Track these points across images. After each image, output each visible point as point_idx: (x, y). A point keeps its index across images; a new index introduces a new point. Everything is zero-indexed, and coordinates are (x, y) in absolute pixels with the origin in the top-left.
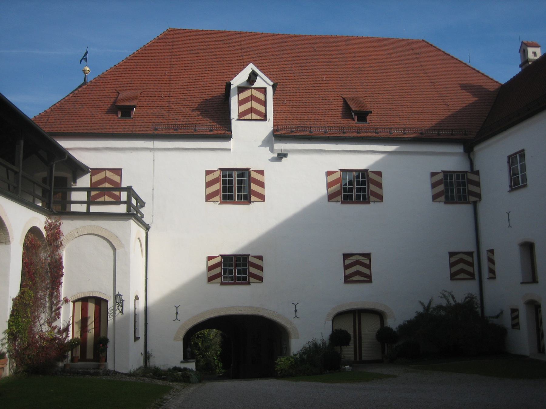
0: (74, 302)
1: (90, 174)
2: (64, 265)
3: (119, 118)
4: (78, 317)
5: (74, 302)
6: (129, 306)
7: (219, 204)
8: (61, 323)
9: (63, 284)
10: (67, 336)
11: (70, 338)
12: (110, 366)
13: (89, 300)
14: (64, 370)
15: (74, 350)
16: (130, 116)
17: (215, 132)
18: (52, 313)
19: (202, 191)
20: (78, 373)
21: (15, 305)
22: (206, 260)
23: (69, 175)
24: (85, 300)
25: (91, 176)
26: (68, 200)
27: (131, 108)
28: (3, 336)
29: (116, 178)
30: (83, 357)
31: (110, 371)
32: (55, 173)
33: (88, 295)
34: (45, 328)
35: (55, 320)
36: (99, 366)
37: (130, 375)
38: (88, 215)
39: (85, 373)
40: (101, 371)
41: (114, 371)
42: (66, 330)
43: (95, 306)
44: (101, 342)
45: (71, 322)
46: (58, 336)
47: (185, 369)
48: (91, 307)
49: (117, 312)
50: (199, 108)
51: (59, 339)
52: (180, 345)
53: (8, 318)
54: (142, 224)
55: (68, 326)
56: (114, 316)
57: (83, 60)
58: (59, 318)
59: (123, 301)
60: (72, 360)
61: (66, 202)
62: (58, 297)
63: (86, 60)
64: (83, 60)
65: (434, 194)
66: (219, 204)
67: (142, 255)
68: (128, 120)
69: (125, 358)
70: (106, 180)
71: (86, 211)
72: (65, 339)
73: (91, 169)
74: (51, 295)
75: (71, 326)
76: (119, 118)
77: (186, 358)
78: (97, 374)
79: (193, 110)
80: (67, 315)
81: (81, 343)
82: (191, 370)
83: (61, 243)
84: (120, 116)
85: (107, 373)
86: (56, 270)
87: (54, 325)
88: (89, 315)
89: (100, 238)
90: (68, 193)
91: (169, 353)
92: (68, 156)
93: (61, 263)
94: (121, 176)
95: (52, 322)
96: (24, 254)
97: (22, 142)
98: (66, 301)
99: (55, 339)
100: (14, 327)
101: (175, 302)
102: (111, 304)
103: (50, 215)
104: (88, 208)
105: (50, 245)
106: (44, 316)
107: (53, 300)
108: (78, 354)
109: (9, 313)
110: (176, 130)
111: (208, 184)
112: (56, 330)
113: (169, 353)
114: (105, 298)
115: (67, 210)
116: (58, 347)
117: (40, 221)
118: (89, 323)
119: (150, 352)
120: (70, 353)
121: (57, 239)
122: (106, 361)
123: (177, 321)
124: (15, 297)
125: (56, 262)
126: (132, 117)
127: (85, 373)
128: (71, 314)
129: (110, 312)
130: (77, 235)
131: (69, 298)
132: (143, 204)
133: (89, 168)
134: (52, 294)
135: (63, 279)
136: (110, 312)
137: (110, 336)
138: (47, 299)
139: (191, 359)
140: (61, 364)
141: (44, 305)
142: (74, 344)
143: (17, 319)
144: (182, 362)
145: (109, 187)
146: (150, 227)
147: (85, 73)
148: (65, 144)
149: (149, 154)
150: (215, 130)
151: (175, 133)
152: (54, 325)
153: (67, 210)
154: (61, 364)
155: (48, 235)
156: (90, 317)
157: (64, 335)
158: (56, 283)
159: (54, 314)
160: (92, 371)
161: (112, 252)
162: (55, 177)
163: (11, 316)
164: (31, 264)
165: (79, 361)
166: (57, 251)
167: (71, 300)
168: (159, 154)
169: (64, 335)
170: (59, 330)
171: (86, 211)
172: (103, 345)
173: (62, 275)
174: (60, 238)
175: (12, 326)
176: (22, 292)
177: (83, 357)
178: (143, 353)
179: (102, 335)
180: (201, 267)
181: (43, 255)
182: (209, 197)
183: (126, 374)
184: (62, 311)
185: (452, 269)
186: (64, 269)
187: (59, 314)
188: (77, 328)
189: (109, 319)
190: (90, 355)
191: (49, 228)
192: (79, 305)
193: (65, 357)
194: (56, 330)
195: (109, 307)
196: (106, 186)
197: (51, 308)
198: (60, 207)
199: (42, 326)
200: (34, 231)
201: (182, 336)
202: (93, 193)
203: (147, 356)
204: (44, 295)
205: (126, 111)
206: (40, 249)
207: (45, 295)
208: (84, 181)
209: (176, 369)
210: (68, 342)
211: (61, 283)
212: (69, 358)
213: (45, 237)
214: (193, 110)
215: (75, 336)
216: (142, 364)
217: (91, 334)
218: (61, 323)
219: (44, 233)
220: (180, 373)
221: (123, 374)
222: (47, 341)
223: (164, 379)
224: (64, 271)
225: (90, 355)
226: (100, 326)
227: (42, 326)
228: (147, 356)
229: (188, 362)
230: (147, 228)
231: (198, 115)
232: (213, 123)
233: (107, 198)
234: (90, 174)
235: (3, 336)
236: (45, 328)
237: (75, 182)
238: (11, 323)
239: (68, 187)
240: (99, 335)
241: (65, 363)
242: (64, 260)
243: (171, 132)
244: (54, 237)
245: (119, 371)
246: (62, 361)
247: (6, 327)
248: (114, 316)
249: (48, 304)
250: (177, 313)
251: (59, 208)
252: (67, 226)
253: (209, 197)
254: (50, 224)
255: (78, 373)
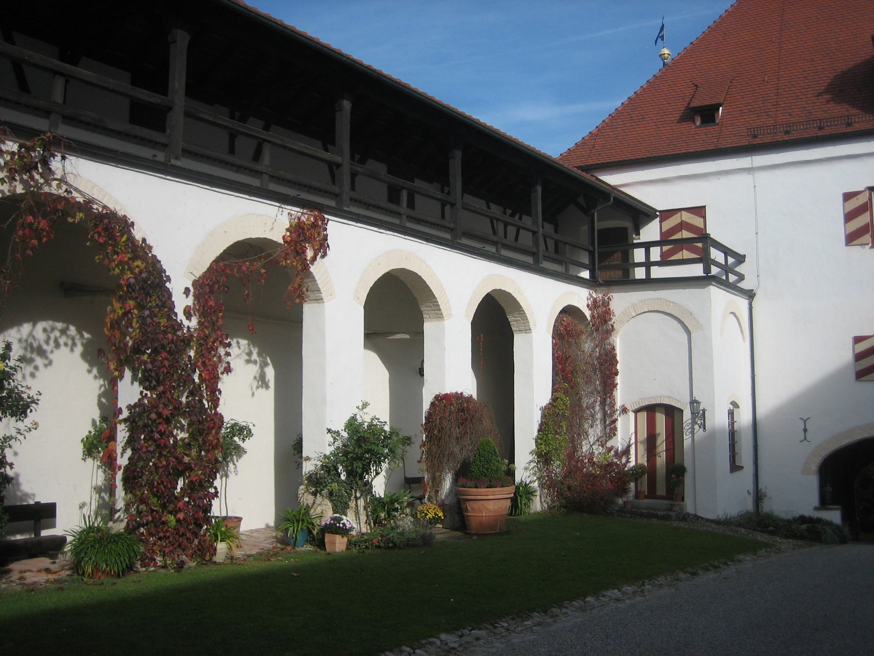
0: (636, 412)
1: (658, 219)
2: (618, 358)
3: (698, 127)
4: (643, 434)
5: (636, 412)
6: (718, 419)
7: (871, 247)
8: (619, 442)
9: (618, 387)
10: (628, 461)
11: (632, 464)
12: (689, 508)
13: (657, 409)
14: (622, 511)
15: (639, 481)
16: (714, 121)
17: (857, 127)
18: (605, 428)
19: (839, 229)
20: (641, 515)
21: (543, 416)
22: (851, 342)
23: (628, 224)
24: (651, 409)
25: (661, 222)
26: (630, 261)
27: (716, 108)
28: (530, 458)
29: (697, 221)
30: (652, 493)
31: (688, 514)
32: (598, 226)
33: (653, 402)
34: (598, 450)
35: (610, 437)
36: (672, 505)
37: (718, 522)
38: (649, 282)
39: (649, 516)
40: (673, 514)
41: (695, 515)
42: (626, 452)
43: (663, 417)
44: (676, 472)
45: (633, 441)
46: (615, 460)
47: (819, 520)
48: (661, 419)
49: (696, 427)
50: (827, 91)
51: (616, 464)
52: (813, 481)
53: (536, 433)
54: (736, 291)
55: (629, 446)
56: (693, 433)
57: (659, 39)
58: (615, 435)
59: (704, 411)
60: (637, 495)
61: (628, 264)
62: (612, 405)
63: (662, 38)
64: (659, 39)
65: (848, 232)
66: (871, 247)
67: (744, 338)
68: (710, 129)
69: (717, 495)
70: (682, 225)
71: (644, 277)
72: (625, 465)
73: (660, 211)
74: (603, 403)
75: (633, 446)
76: (698, 127)
77: (824, 503)
78: (667, 518)
79: (819, 95)
80: (627, 431)
81: (648, 472)
82: (829, 523)
83: (612, 326)
84: (698, 123)
85: (685, 517)
86: (607, 367)
87: (609, 444)
88: (658, 431)
89: (667, 317)
90: (630, 251)
91: (797, 494)
92: (615, 198)
93: (614, 356)
94: (704, 217)
95: (606, 441)
96: (554, 346)
97: (539, 189)
98: (624, 410)
99: (611, 464)
100: (543, 447)
101: (802, 411)
102: (687, 415)
103: (595, 286)
104: (648, 272)
105: (597, 330)
106: (594, 432)
107: (606, 408)
108: (645, 488)
109: (536, 427)
110: (787, 133)
111: (849, 217)
112: (612, 453)
113: (797, 494)
114: (678, 406)
115: (631, 278)
116: (616, 477)
117: (579, 297)
118: (658, 444)
119: (763, 491)
120: (632, 485)
121: (606, 321)
122: (683, 500)
123: (805, 442)
124: (544, 405)
125: (606, 355)
126: (717, 121)
127: (649, 516)
128: (632, 430)
129: (687, 428)
130: (634, 314)
131: (628, 406)
132: (740, 259)
133: (656, 211)
134: (605, 400)
135: (619, 379)
136: (686, 427)
137: (687, 464)
138: (597, 408)
139: (832, 504)
140: (620, 501)
141: (593, 416)
142: (637, 473)
143: (546, 435)
144: (816, 509)
145: (690, 239)
146: (755, 294)
147: (663, 59)
148: (612, 179)
149: (746, 178)
150: (855, 122)
151: (786, 138)
152: (609, 444)
153: (631, 278)
154: (620, 501)
155: (593, 316)
156: (659, 434)
157: (624, 460)
158: (608, 386)
159: (608, 430)
160: (660, 513)
161: (685, 336)
162: (599, 231)
163: (539, 431)
164: (567, 359)
165: (646, 497)
166: (607, 338)
167: (631, 409)
168: (763, 177)
169: (624, 460)
170: (616, 452)
171: (644, 277)
172: (678, 476)
173: (616, 374)
174: (610, 319)
175: (541, 444)
176: (554, 399)
177: (652, 493)
178: (751, 491)
179: (677, 461)
180: (843, 355)
181: (587, 346)
182: (851, 238)
183: (712, 521)
184: (619, 424)
185: (856, 346)
186: (618, 365)
187: (615, 429)
188: (642, 449)
189: (685, 437)
190: (661, 490)
191: (594, 305)
192: (643, 416)
193: (625, 491)
194: (612, 453)
195: (684, 420)
196: (684, 237)
197: (604, 420)
198: (621, 273)
199: (590, 445)
200: (569, 311)
201: (814, 467)
202: (665, 248)
203: (758, 497)
204: (590, 400)
205: (708, 114)
206: (584, 337)
207: (595, 401)
208: (651, 232)
209: (803, 519)
210: (631, 469)
211: (615, 386)
212: (632, 494)
213: (589, 318)
214: (819, 95)
215: (639, 462)
216: (750, 506)
217: (661, 459)
218: (619, 442)
219: (588, 313)
220: (804, 527)
221: (707, 520)
222: (600, 467)
223: (772, 533)
224: (618, 367)
225: (661, 490)
226: (674, 448)
227: (590, 445)
228: (758, 497)
229: (827, 509)
230: (750, 295)
231: (828, 102)
232: (854, 111)
233: (686, 254)
234: (658, 219)
235: (530, 458)
236: (598, 450)
237: (638, 234)
238: (539, 441)
239: (630, 242)
240: (674, 461)
241: (625, 499)
242: (618, 351)
243: (780, 137)
244: (603, 318)
245: (703, 516)
246: (621, 497)
247: (533, 446)
248: (693, 433)
249: (599, 416)
250: (805, 430)
251: (618, 274)
252: (621, 301)
253: (851, 238)
254: (595, 301)
255: (641, 515)
